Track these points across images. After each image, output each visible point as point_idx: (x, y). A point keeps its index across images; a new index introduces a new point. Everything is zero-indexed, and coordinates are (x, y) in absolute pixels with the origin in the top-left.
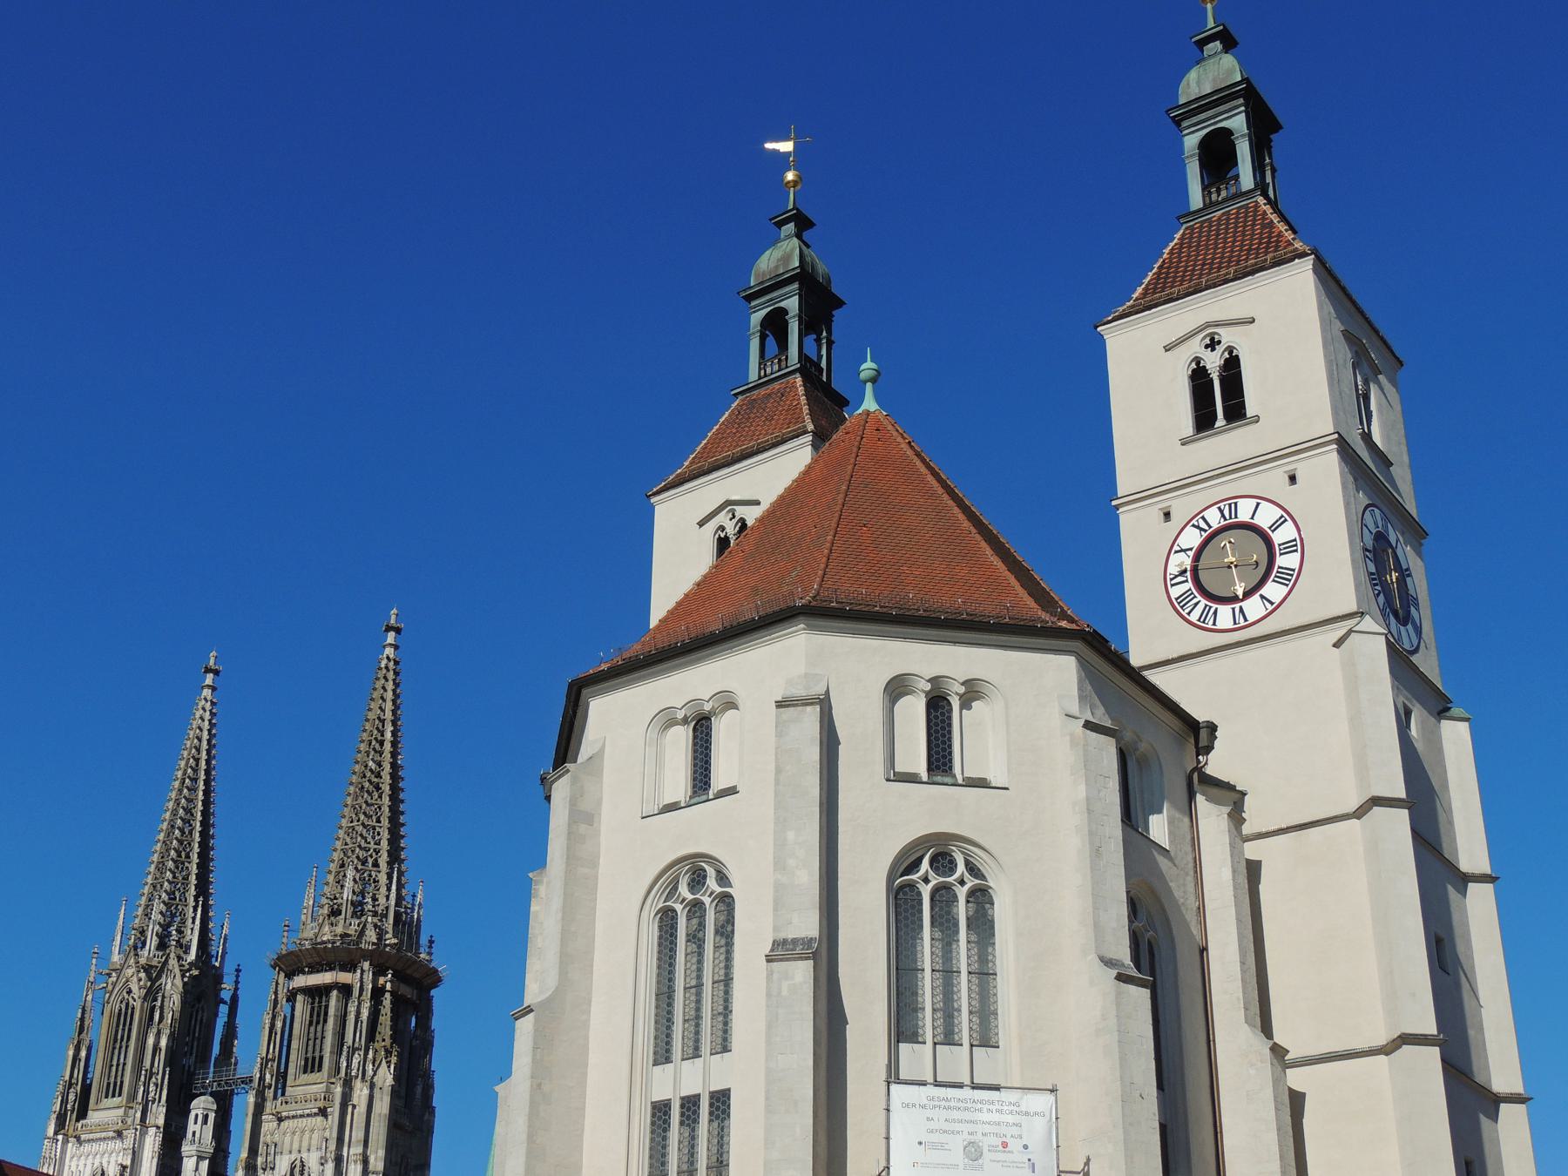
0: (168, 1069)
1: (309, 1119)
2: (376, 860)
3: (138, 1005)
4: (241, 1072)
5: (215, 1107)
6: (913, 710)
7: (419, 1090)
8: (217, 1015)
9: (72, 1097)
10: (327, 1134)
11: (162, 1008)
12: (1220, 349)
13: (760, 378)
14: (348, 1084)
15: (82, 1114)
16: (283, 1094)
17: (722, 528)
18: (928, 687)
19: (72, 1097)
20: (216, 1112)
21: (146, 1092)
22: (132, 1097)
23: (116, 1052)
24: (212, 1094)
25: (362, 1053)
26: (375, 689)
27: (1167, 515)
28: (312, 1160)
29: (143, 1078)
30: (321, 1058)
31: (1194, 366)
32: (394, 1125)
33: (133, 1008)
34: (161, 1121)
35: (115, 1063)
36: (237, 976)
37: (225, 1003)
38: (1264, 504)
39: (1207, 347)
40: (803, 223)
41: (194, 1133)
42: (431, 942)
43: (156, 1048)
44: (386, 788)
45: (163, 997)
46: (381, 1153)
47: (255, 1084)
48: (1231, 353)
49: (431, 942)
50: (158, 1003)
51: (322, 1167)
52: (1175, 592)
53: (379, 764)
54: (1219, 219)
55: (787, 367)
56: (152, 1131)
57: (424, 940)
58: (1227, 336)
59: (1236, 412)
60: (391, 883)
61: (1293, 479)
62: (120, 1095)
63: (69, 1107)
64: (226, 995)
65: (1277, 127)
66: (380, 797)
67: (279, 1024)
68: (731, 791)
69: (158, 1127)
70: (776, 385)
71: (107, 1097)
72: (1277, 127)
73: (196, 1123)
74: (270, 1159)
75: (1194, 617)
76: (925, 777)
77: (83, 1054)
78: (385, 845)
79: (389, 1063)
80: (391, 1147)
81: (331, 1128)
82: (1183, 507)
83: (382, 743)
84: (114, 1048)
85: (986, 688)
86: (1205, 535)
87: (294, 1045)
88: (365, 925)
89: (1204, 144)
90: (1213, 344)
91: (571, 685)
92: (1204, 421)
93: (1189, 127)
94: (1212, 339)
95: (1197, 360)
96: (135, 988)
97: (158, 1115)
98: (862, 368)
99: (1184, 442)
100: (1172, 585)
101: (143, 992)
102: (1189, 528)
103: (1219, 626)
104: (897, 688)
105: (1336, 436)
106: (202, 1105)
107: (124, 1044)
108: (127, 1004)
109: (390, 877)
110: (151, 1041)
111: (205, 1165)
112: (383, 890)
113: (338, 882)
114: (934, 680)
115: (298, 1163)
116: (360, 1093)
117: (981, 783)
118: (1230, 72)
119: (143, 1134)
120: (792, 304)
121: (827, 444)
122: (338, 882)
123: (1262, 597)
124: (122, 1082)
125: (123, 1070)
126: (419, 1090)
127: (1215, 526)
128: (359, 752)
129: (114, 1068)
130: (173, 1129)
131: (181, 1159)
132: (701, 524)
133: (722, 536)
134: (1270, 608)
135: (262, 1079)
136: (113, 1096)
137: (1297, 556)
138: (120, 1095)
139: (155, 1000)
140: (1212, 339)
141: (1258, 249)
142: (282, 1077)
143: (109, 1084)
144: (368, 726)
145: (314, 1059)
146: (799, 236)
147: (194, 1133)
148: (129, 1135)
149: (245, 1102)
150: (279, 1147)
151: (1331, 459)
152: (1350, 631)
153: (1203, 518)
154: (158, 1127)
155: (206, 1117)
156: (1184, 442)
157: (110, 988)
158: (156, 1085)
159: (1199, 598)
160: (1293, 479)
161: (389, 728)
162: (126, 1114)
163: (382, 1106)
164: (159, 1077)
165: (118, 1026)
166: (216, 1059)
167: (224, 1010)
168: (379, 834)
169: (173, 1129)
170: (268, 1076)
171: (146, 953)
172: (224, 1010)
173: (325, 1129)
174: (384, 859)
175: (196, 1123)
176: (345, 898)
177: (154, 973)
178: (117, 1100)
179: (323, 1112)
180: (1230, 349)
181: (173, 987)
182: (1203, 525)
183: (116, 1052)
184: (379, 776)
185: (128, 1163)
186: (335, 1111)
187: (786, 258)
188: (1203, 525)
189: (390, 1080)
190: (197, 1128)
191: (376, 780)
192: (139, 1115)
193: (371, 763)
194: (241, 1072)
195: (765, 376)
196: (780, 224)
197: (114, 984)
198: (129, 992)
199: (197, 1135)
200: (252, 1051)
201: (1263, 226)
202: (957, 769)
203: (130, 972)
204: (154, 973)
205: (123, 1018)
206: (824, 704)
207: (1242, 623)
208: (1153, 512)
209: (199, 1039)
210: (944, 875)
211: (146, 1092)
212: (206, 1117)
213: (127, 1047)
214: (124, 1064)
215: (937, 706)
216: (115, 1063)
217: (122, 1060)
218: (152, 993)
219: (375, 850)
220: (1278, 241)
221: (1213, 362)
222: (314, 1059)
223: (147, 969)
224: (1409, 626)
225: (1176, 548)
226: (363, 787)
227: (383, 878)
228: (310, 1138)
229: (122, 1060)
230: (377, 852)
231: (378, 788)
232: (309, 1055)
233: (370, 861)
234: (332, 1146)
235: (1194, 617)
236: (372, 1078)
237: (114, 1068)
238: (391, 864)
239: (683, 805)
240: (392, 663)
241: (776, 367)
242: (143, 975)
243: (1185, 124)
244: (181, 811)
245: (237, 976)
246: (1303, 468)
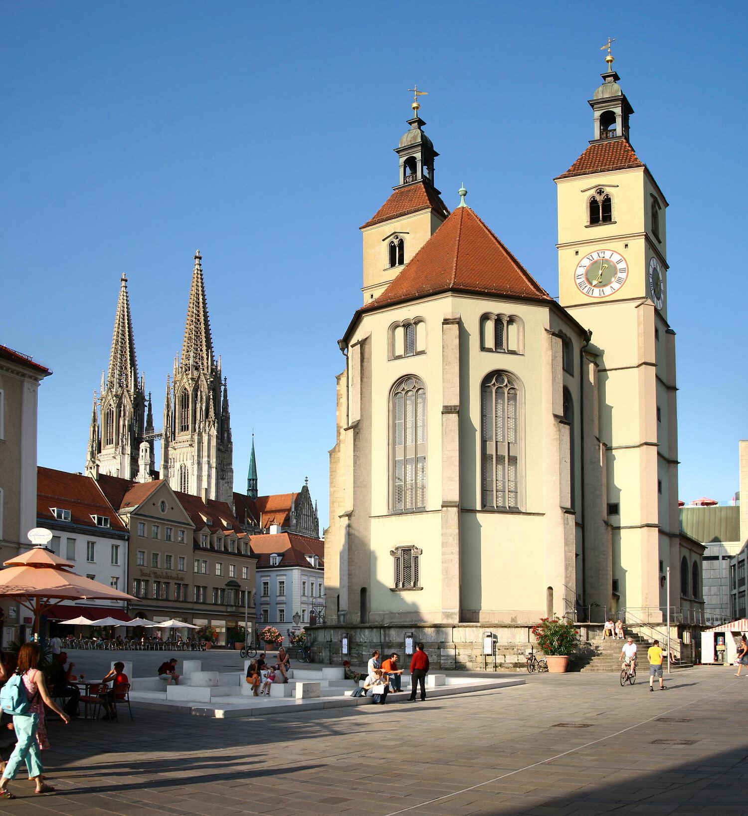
0: (129, 433)
1: (186, 448)
2: (201, 349)
3: (114, 410)
4: (156, 432)
5: (149, 446)
6: (490, 326)
7: (226, 435)
8: (144, 411)
9: (94, 446)
10: (193, 454)
11: (124, 410)
12: (603, 195)
13: (404, 184)
14: (200, 434)
15: (99, 452)
16: (174, 440)
17: (393, 242)
18: (496, 317)
19: (94, 446)
20: (149, 448)
21: (122, 441)
22: (117, 444)
23: (109, 428)
24: (146, 441)
25: (204, 423)
26: (193, 282)
27: (577, 253)
28: (189, 464)
29: (120, 437)
30: (188, 425)
31: (592, 199)
32: (218, 450)
33: (113, 411)
34: (129, 453)
35: (109, 432)
36: (150, 396)
37: (146, 406)
38: (615, 254)
39: (598, 193)
40: (421, 123)
41: (142, 456)
42: (225, 379)
43: (124, 425)
44: (203, 322)
45: (124, 406)
46: (215, 460)
47: (164, 436)
48: (607, 196)
49: (225, 379)
50: (122, 409)
51: (192, 466)
52: (578, 281)
53: (198, 312)
54: (606, 145)
55: (416, 180)
56: (127, 456)
57: (223, 378)
58: (608, 190)
59: (608, 219)
60: (208, 357)
61: (626, 246)
62: (112, 444)
63: (94, 449)
64: (147, 403)
65: (632, 112)
66: (200, 324)
67: (170, 414)
68: (422, 353)
69: (128, 455)
70: (412, 187)
71: (107, 445)
72: (632, 112)
73: (143, 452)
74: (172, 464)
75: (585, 291)
76: (494, 350)
77: (97, 429)
78: (204, 342)
79: (214, 426)
80: (218, 457)
81: (195, 452)
82: (584, 250)
83: (199, 303)
84: (108, 426)
85: (517, 319)
86: (591, 262)
87: (177, 421)
88: (200, 374)
89: (602, 116)
90: (600, 192)
91: (357, 312)
92: (594, 220)
93: (596, 108)
94: (601, 191)
95: (594, 197)
96: (112, 404)
97: (128, 450)
98: (460, 190)
99: (586, 227)
100: (577, 279)
101: (116, 405)
102: (585, 258)
103: (594, 295)
104: (485, 317)
105: (645, 233)
106: (144, 445)
107: (111, 425)
108: (110, 410)
109: (207, 355)
110: (121, 423)
111: (148, 467)
112: (205, 359)
113: (187, 358)
114: (498, 315)
115: (183, 465)
116: (205, 438)
117: (513, 353)
118: (617, 91)
119: (124, 458)
120: (418, 156)
121: (447, 219)
122: (187, 358)
123: (611, 287)
124: (112, 439)
125: (112, 434)
126: (226, 435)
127: (595, 259)
128: (190, 307)
129: (109, 434)
130: (134, 455)
131: (138, 466)
132: (384, 240)
133: (393, 245)
134: (614, 291)
135: (166, 434)
136: (110, 444)
137: (626, 274)
138: (112, 444)
139: (121, 407)
140: (601, 191)
141: (622, 159)
142: (174, 433)
143: (107, 440)
144: (192, 297)
145: (185, 426)
146: (419, 128)
147: (142, 456)
148: (118, 457)
149: (159, 444)
150: (175, 459)
151: (642, 242)
152: (643, 304)
153: (591, 256)
154: (128, 455)
155: (146, 450)
156: (586, 227)
157: (103, 404)
158: (126, 439)
159: (587, 284)
160: (626, 246)
161: (201, 297)
162: (116, 450)
163: (214, 442)
164: (127, 436)
165: (108, 418)
166: (146, 428)
167: (146, 409)
168: (201, 339)
169: (134, 455)
170: (168, 433)
171: (115, 390)
172: (146, 409)
173: (192, 452)
174: (204, 348)
175: (143, 452)
176: (191, 364)
177: (119, 398)
178: (112, 445)
179: (191, 445)
180: (607, 195)
181: (128, 403)
182: (591, 258)
183: (109, 428)
184: (199, 316)
185: (119, 468)
186: (196, 445)
187: (415, 137)
188: (591, 258)
189: (215, 433)
190: (143, 454)
191: (198, 318)
192: (121, 450)
193: (195, 311)
194: (156, 432)
195: (407, 183)
196: (410, 124)
197: (104, 403)
198: (110, 405)
199: (144, 457)
200: (160, 424)
201: (625, 151)
202: (505, 346)
203: (109, 398)
204: (119, 398)
205: (108, 415)
206: (459, 322)
207: (603, 295)
208: (572, 251)
209: (139, 421)
210: (500, 384)
211: (122, 441)
212: (146, 450)
213: (112, 425)
214: (112, 432)
215: (499, 321)
216: (109, 432)
217: (111, 431)
218: (119, 405)
219: (200, 345)
220: (630, 158)
221: (600, 199)
222: (185, 426)
223: (116, 396)
224: (660, 301)
225: (580, 265)
226: (193, 321)
227: (205, 357)
228: (187, 456)
229: (111, 431)
230: (201, 346)
231: (199, 321)
232: (183, 425)
233: (199, 349)
234: (196, 458)
235: (585, 291)
236: (209, 432)
237: (109, 434)
238: (207, 350)
239: (403, 356)
240: (199, 271)
241: (411, 179)
242: (114, 398)
243: (595, 106)
244: (120, 327)
245: (150, 396)
246: (631, 243)
